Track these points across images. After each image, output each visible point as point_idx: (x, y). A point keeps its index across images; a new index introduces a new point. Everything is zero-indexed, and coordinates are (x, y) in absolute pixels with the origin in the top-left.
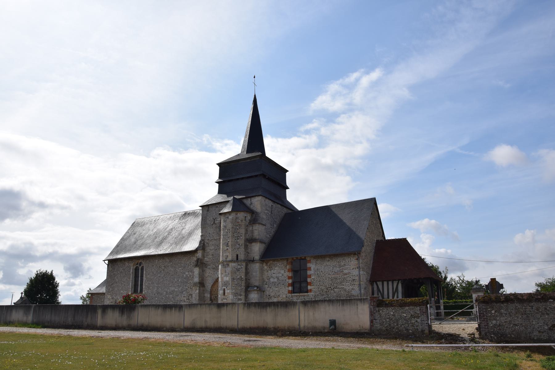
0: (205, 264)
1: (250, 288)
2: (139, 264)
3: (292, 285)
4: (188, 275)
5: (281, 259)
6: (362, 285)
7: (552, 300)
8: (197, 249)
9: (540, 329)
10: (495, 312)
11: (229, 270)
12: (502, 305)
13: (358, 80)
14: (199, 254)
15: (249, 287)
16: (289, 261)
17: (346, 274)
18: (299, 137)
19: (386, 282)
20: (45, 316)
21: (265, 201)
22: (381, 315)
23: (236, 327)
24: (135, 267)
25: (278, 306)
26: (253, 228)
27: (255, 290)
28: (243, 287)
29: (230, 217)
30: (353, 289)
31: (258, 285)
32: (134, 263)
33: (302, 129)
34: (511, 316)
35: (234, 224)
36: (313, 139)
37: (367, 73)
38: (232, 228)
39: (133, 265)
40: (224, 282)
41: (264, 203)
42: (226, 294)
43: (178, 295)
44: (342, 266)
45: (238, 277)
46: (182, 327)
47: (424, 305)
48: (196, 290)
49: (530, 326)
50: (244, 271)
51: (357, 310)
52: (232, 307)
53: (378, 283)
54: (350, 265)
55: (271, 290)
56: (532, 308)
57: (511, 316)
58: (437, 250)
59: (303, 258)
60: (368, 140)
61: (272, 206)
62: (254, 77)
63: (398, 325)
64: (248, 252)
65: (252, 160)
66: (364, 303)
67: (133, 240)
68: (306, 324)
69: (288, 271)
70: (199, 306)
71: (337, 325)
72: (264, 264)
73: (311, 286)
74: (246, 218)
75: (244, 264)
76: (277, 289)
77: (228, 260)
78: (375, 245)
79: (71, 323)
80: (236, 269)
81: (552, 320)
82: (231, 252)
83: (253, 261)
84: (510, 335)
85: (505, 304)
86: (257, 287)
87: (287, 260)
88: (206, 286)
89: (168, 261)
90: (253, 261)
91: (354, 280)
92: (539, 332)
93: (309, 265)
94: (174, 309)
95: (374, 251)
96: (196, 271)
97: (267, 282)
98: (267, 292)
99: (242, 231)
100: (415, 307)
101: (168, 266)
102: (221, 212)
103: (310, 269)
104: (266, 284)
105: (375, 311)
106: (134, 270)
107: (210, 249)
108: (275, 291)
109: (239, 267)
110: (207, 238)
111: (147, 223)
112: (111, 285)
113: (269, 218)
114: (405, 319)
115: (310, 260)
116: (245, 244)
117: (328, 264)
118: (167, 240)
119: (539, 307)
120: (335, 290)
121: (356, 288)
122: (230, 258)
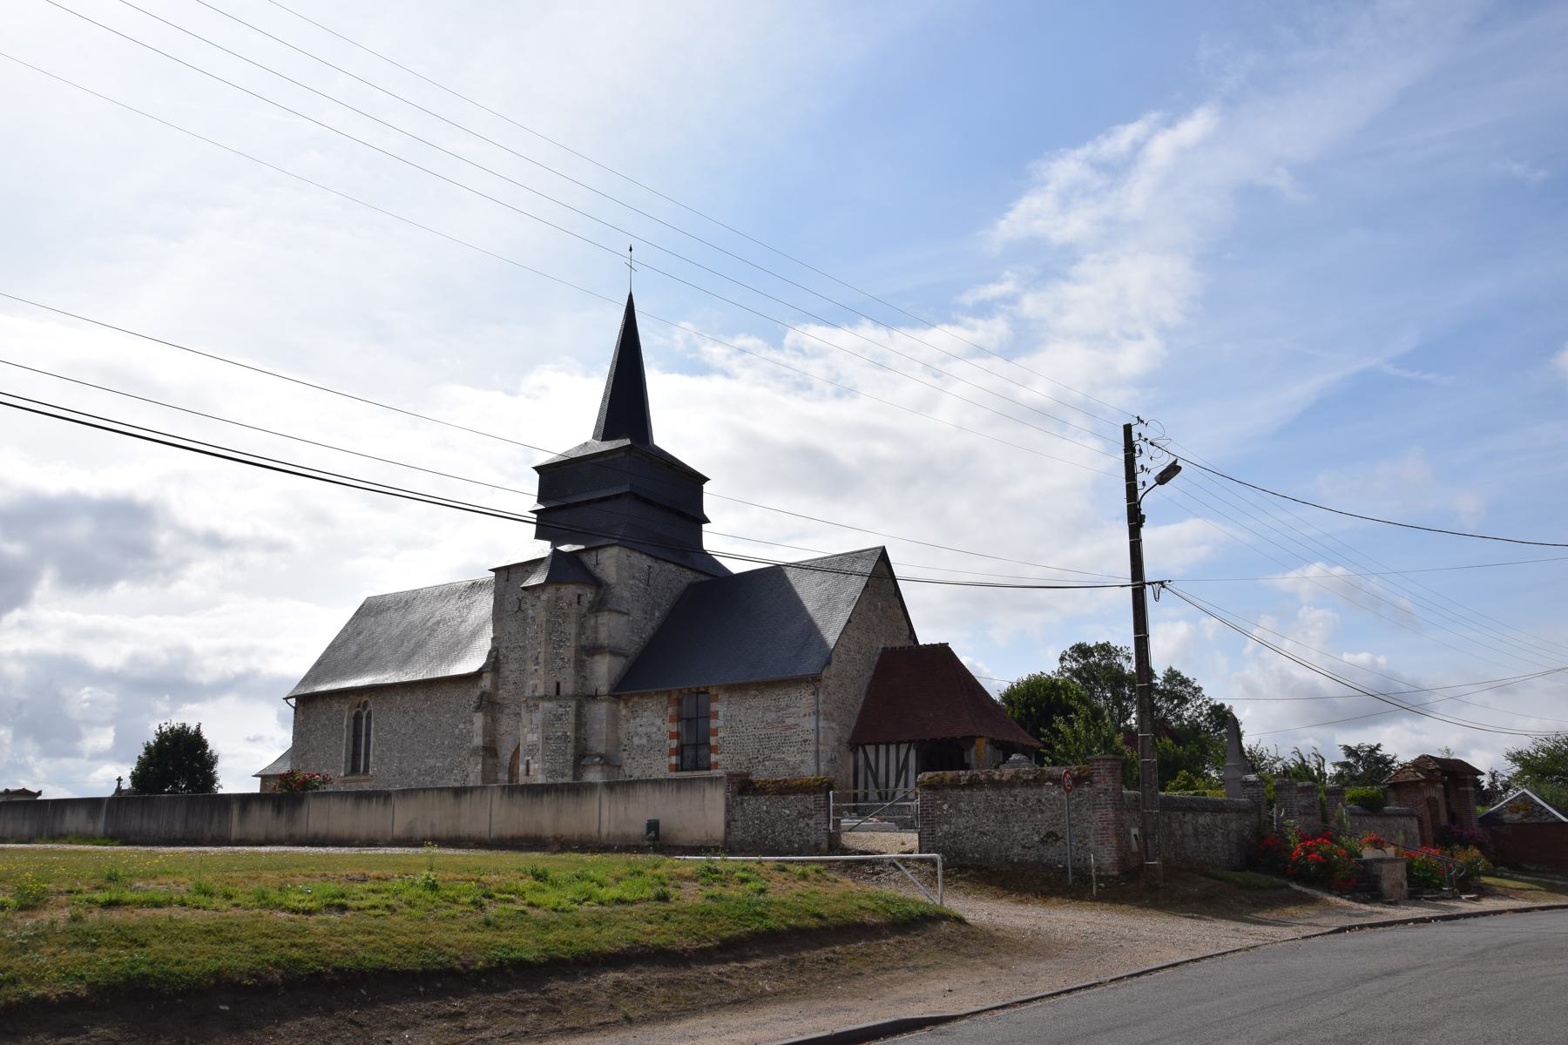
0: (498, 704)
1: (587, 759)
2: (362, 705)
3: (679, 751)
4: (465, 731)
5: (657, 693)
6: (823, 752)
7: (1051, 784)
8: (480, 669)
9: (1025, 841)
10: (950, 807)
11: (538, 717)
12: (962, 793)
13: (1138, 147)
14: (486, 683)
15: (584, 757)
16: (674, 696)
17: (789, 728)
18: (954, 323)
19: (873, 747)
20: (131, 821)
21: (630, 557)
22: (744, 812)
23: (487, 836)
24: (354, 713)
25: (562, 791)
26: (597, 621)
27: (595, 764)
28: (570, 758)
29: (544, 597)
30: (802, 762)
31: (603, 752)
32: (350, 702)
33: (968, 299)
34: (976, 816)
35: (551, 613)
36: (999, 328)
37: (1170, 124)
38: (548, 621)
39: (350, 708)
40: (528, 746)
41: (627, 562)
42: (531, 773)
43: (443, 775)
44: (783, 709)
45: (560, 734)
46: (389, 838)
47: (821, 792)
48: (477, 764)
49: (1009, 836)
50: (574, 721)
51: (704, 802)
52: (481, 794)
53: (867, 748)
54: (799, 707)
55: (634, 765)
56: (1016, 800)
57: (976, 816)
58: (1347, 657)
59: (702, 689)
60: (1162, 330)
61: (650, 567)
62: (631, 250)
63: (773, 832)
64: (584, 677)
65: (610, 457)
66: (716, 786)
67: (354, 648)
68: (612, 831)
69: (671, 721)
70: (421, 793)
71: (661, 831)
72: (622, 705)
73: (718, 754)
74: (582, 597)
75: (573, 704)
76: (646, 761)
77: (537, 694)
78: (877, 659)
79: (179, 836)
80: (554, 715)
81: (1047, 823)
82: (543, 677)
83: (594, 697)
84: (973, 853)
85: (968, 792)
86: (602, 757)
87: (669, 696)
88: (501, 755)
89: (423, 698)
90: (594, 697)
91: (805, 741)
92: (1024, 847)
93: (714, 706)
94: (374, 800)
95: (871, 673)
96: (479, 720)
97: (626, 746)
98: (626, 769)
99: (571, 629)
100: (807, 796)
101: (423, 711)
102: (524, 585)
103: (716, 715)
104: (625, 750)
105: (735, 804)
106: (352, 721)
107: (510, 669)
108: (643, 766)
109: (561, 710)
110: (504, 645)
111: (389, 608)
112: (303, 754)
113: (639, 596)
114: (787, 820)
115: (717, 695)
116: (576, 657)
117: (753, 704)
118: (424, 649)
119: (1028, 798)
120: (767, 763)
121: (811, 762)
122: (540, 691)
